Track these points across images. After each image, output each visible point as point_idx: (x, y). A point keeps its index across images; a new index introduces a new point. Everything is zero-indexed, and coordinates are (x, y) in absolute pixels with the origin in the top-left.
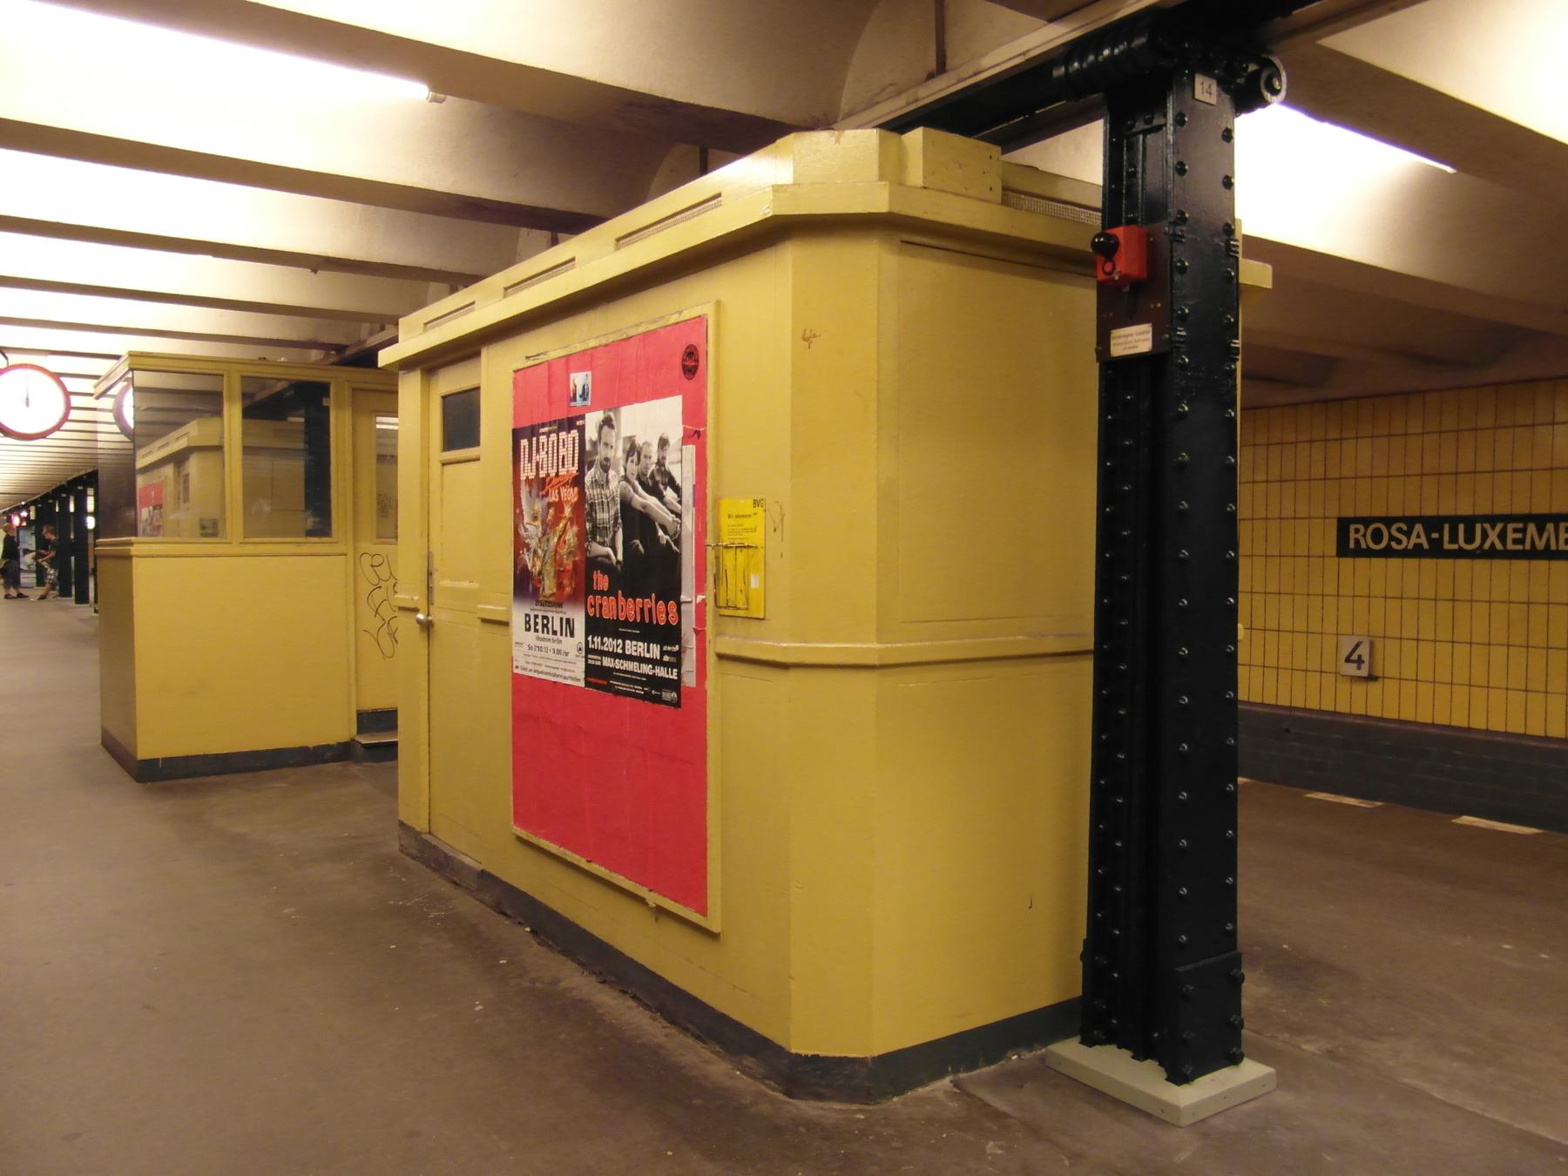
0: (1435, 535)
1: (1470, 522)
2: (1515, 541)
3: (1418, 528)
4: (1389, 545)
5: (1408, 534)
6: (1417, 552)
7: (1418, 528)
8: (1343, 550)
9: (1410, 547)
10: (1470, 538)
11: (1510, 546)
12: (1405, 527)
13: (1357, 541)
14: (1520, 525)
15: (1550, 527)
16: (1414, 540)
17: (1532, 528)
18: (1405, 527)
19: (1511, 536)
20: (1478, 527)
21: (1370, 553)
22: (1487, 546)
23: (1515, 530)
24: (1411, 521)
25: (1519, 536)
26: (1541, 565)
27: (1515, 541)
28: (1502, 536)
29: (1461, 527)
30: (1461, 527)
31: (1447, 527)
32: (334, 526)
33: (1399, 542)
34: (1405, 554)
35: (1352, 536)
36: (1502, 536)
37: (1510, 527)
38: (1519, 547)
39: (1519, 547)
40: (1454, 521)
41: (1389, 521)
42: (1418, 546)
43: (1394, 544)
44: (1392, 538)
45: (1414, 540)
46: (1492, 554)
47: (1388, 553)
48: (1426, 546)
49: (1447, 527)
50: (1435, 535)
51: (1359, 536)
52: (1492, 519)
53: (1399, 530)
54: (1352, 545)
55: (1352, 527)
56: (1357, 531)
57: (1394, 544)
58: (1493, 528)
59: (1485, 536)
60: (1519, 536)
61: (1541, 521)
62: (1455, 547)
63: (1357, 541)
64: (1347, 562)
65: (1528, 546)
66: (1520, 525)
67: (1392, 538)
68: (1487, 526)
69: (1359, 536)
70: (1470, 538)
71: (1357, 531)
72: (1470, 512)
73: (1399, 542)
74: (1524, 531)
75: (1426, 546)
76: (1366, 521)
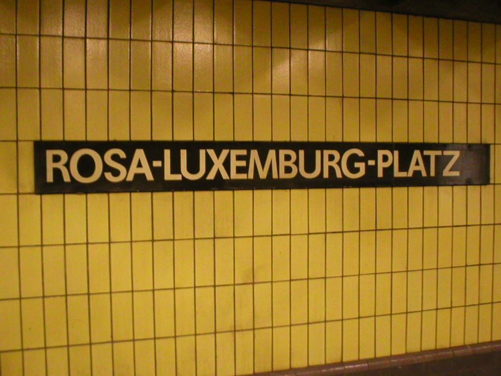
0: (157, 164)
1: (193, 147)
2: (240, 170)
3: (140, 154)
4: (103, 176)
5: (127, 163)
6: (139, 184)
7: (140, 154)
8: (42, 188)
9: (130, 178)
10: (193, 167)
11: (234, 175)
12: (122, 155)
13: (57, 173)
14: (244, 152)
15: (272, 154)
16: (134, 169)
17: (254, 154)
18: (122, 155)
19: (234, 164)
20: (202, 153)
21: (76, 188)
22: (211, 176)
23: (239, 158)
24: (130, 147)
25: (243, 163)
26: (263, 195)
27: (240, 170)
28: (227, 164)
29: (184, 153)
30: (184, 153)
31: (167, 153)
32: (235, 168)
33: (116, 173)
34: (125, 187)
35: (50, 166)
36: (227, 164)
37: (234, 153)
38: (243, 176)
39: (243, 176)
40: (175, 146)
41: (101, 147)
42: (140, 177)
43: (109, 176)
44: (106, 168)
45: (134, 169)
46: (219, 184)
47: (102, 187)
48: (150, 177)
49: (167, 153)
50: (157, 164)
51: (290, 164)
52: (218, 146)
53: (115, 158)
54: (50, 178)
55: (50, 154)
56: (57, 159)
57: (109, 176)
58: (218, 155)
59: (210, 164)
60: (243, 163)
61: (263, 148)
62: (178, 177)
63: (57, 173)
64: (52, 201)
65: (251, 175)
66: (244, 152)
67: (106, 168)
68: (211, 152)
69: (60, 165)
70: (193, 167)
71: (331, 158)
72: (405, 140)
73: (116, 173)
74: (247, 158)
75: (150, 177)
76: (71, 147)
